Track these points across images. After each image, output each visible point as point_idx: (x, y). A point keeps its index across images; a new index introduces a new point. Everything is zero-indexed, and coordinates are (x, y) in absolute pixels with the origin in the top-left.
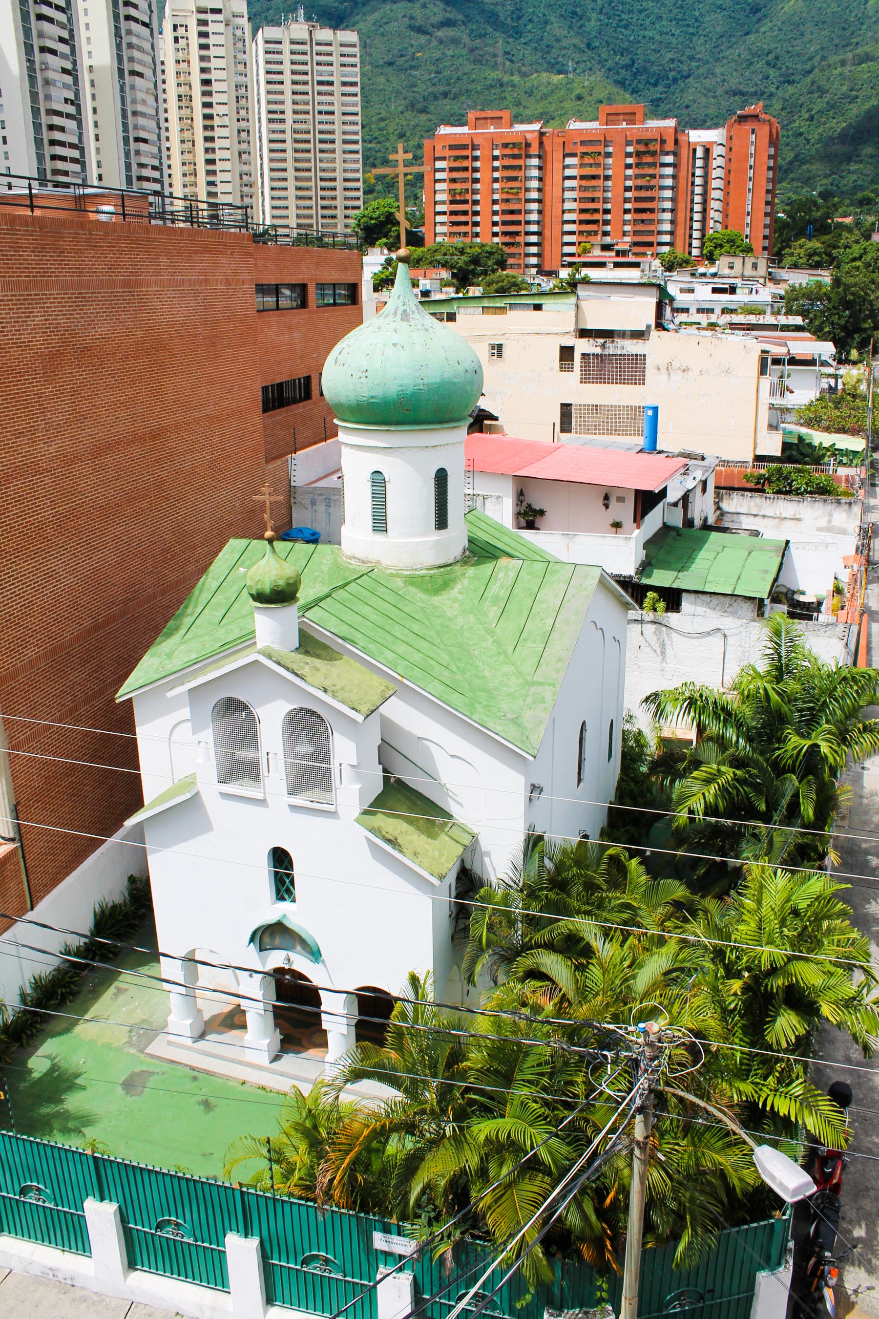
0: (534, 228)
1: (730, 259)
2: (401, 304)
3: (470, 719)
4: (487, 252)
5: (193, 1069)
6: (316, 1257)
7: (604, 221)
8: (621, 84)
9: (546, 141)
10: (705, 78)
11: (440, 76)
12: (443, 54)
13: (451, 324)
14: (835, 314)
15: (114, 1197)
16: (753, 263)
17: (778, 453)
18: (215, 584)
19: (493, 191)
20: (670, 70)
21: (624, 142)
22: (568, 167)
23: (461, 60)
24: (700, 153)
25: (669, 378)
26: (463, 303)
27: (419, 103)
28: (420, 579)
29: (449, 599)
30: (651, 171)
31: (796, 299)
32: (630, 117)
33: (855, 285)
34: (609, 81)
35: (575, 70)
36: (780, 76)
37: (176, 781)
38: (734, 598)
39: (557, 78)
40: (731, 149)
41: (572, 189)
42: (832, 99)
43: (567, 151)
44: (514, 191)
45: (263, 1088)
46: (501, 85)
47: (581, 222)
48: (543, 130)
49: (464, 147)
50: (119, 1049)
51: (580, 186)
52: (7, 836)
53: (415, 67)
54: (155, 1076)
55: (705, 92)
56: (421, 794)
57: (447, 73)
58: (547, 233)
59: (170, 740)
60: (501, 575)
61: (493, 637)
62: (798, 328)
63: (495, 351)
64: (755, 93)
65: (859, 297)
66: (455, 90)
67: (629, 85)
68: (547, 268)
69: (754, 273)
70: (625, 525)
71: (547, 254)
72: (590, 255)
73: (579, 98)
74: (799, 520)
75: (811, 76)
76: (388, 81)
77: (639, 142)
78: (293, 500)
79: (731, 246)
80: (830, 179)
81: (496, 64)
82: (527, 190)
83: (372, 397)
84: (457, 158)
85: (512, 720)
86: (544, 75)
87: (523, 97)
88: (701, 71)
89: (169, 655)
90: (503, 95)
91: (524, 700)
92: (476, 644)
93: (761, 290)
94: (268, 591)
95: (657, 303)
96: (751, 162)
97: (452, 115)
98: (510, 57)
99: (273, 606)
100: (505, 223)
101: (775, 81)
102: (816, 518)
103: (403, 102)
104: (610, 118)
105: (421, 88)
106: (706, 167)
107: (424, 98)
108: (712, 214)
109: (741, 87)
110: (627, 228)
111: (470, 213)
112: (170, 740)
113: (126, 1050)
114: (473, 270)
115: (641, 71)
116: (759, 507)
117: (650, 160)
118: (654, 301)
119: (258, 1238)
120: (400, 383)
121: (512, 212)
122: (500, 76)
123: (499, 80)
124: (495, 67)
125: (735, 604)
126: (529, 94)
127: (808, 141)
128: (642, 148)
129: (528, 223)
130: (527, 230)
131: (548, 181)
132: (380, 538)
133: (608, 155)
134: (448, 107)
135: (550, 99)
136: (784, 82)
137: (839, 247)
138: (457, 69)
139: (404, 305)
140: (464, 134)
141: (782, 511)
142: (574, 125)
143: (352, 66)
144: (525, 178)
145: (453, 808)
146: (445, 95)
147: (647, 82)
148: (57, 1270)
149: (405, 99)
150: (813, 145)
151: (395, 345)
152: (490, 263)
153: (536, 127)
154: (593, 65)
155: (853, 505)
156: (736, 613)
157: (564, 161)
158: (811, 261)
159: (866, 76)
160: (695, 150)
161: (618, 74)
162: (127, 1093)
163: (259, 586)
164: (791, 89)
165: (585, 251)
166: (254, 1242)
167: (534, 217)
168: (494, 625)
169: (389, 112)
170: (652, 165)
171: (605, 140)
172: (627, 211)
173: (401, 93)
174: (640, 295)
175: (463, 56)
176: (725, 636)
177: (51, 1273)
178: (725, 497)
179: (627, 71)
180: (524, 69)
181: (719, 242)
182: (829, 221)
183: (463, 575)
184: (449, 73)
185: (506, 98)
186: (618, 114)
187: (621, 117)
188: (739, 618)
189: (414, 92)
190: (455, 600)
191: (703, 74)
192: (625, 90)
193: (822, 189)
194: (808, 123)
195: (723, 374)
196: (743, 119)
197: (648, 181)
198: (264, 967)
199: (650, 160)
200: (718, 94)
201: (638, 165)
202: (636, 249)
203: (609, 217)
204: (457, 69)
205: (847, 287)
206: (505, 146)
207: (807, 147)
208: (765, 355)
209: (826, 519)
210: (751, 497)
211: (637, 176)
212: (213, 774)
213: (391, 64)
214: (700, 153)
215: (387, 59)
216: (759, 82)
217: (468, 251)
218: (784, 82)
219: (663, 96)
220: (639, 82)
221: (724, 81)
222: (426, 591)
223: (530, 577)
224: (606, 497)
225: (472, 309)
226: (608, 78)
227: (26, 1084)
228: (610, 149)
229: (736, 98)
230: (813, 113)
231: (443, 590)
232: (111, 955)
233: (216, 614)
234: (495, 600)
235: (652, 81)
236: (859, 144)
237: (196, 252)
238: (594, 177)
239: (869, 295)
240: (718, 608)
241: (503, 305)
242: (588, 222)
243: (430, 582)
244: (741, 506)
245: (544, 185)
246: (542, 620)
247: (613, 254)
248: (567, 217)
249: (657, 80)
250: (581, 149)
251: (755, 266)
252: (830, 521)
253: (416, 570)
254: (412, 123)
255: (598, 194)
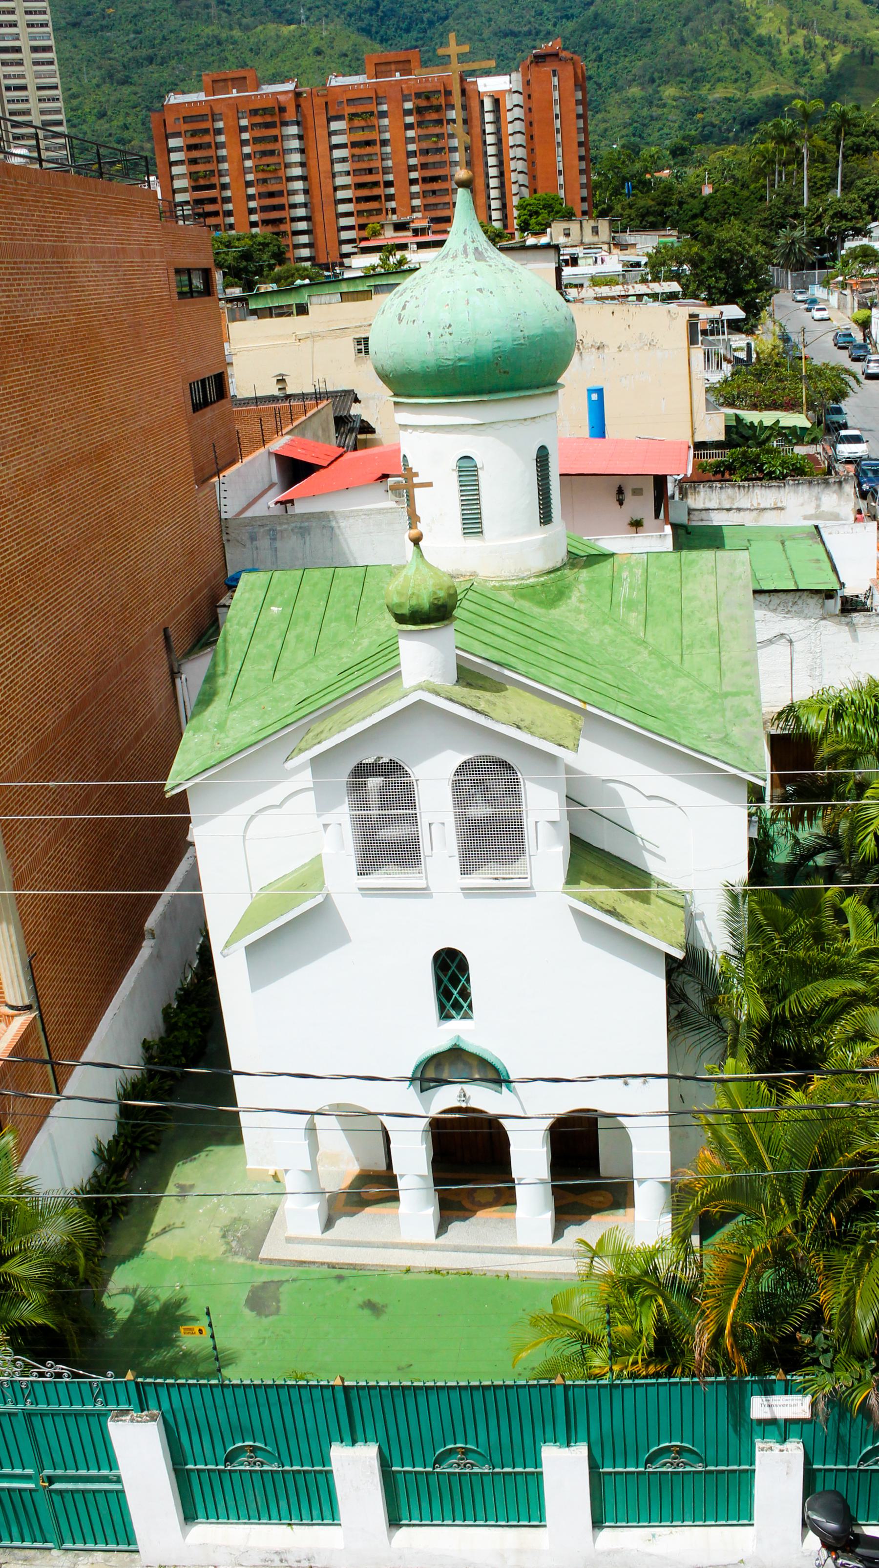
0: (301, 212)
1: (565, 225)
2: (469, 241)
3: (679, 744)
4: (260, 244)
5: (332, 1266)
6: (667, 1449)
7: (386, 196)
8: (366, 31)
9: (304, 104)
10: (467, 18)
11: (141, 36)
12: (140, 8)
13: (302, 318)
14: (711, 277)
15: (370, 1433)
16: (593, 228)
17: (722, 437)
18: (245, 632)
19: (245, 171)
20: (424, 11)
21: (400, 97)
22: (335, 133)
23: (164, 14)
24: (488, 105)
25: (582, 359)
26: (315, 291)
27: (119, 72)
28: (530, 590)
29: (570, 611)
30: (437, 130)
31: (663, 264)
32: (405, 67)
33: (731, 239)
34: (351, 29)
35: (307, 18)
36: (557, 10)
37: (256, 890)
38: (798, 594)
39: (287, 30)
40: (529, 96)
41: (344, 160)
42: (621, 34)
43: (332, 113)
44: (272, 167)
45: (437, 1272)
46: (219, 43)
47: (359, 200)
48: (298, 90)
49: (202, 118)
50: (219, 1262)
51: (353, 156)
52: (20, 1004)
53: (107, 27)
54: (286, 1285)
55: (469, 34)
56: (609, 854)
57: (149, 32)
58: (318, 218)
59: (244, 837)
60: (625, 575)
61: (646, 648)
62: (671, 297)
63: (362, 347)
64: (529, 33)
65: (737, 254)
66: (162, 53)
67: (377, 33)
68: (322, 260)
69: (595, 239)
70: (645, 523)
71: (321, 242)
72: (382, 237)
73: (318, 52)
74: (781, 509)
75: (592, 8)
76: (75, 47)
77: (418, 95)
78: (225, 537)
79: (549, 212)
80: (631, 129)
81: (209, 17)
82: (288, 166)
83: (460, 360)
84: (194, 133)
85: (721, 740)
86: (271, 27)
87: (248, 55)
88: (461, 10)
89: (221, 726)
90: (222, 55)
91: (723, 716)
92: (629, 659)
93: (607, 259)
94: (426, 606)
95: (556, 268)
96: (557, 109)
97: (161, 85)
98: (226, 7)
99: (432, 626)
100: (264, 209)
101: (550, 16)
102: (802, 505)
103: (98, 73)
104: (378, 68)
105: (118, 53)
106: (497, 121)
107: (124, 66)
108: (514, 177)
109: (512, 27)
110: (416, 202)
111: (219, 201)
112: (244, 837)
113: (230, 1260)
114: (246, 268)
115: (389, 13)
116: (732, 499)
117: (434, 116)
118: (553, 266)
119: (586, 1444)
120: (496, 337)
121: (271, 195)
122: (216, 32)
123: (215, 37)
124: (208, 21)
125: (800, 602)
126: (256, 51)
127: (599, 85)
128: (423, 103)
129: (294, 206)
130: (293, 215)
131: (312, 154)
132: (473, 542)
133: (383, 114)
134: (156, 75)
135: (282, 56)
136: (562, 18)
137: (671, 204)
138: (161, 27)
139: (473, 242)
140: (201, 102)
141: (759, 501)
142: (336, 81)
143: (42, 25)
144: (284, 150)
145: (653, 866)
146: (151, 60)
147: (398, 28)
148: (287, 1551)
149: (100, 68)
150: (606, 90)
151: (480, 290)
152: (265, 257)
153: (290, 86)
154: (329, 11)
155: (844, 484)
156: (802, 612)
157: (328, 127)
158: (644, 223)
159: (656, 5)
160: (482, 102)
161: (361, 20)
162: (259, 1314)
163: (414, 602)
164: (570, 25)
165: (375, 234)
166: (580, 1451)
167: (300, 198)
168: (642, 634)
169: (81, 86)
170: (439, 122)
171: (377, 97)
172: (413, 182)
173: (94, 62)
174: (535, 261)
175: (167, 10)
176: (791, 642)
177: (277, 1558)
178: (689, 491)
179: (371, 15)
180: (244, 21)
181: (535, 209)
182: (648, 176)
183: (576, 579)
184: (151, 31)
185: (227, 59)
186: (389, 63)
187: (393, 67)
188: (805, 618)
189: (110, 59)
190: (578, 611)
191: (464, 14)
192: (371, 39)
193: (623, 141)
194: (597, 63)
195: (646, 348)
196: (540, 59)
197: (435, 142)
198: (427, 1112)
199: (434, 116)
200: (485, 36)
201: (420, 124)
202: (435, 227)
203: (392, 191)
204: (161, 27)
205: (722, 243)
206: (254, 112)
207: (599, 92)
208: (694, 320)
209: (814, 504)
210: (721, 488)
211: (421, 138)
212: (351, 862)
213: (75, 25)
214: (488, 105)
215: (70, 19)
216: (532, 19)
217: (237, 244)
218: (562, 18)
219: (420, 43)
220: (388, 28)
221: (490, 20)
222: (540, 603)
223: (663, 572)
224: (620, 491)
225: (328, 297)
226: (349, 25)
227: (115, 1330)
228: (385, 108)
229: (508, 40)
230: (601, 51)
231: (559, 600)
232: (153, 1147)
233: (263, 668)
234: (631, 605)
235: (404, 26)
236: (659, 86)
237: (111, 213)
238: (368, 143)
239: (748, 251)
240: (780, 609)
241: (366, 288)
242: (368, 199)
243: (543, 592)
244: (710, 500)
245: (308, 158)
246: (701, 620)
247: (410, 233)
248: (341, 195)
249: (410, 24)
250: (349, 110)
251: (595, 231)
252: (818, 507)
253: (523, 579)
254: (113, 98)
255: (376, 164)
